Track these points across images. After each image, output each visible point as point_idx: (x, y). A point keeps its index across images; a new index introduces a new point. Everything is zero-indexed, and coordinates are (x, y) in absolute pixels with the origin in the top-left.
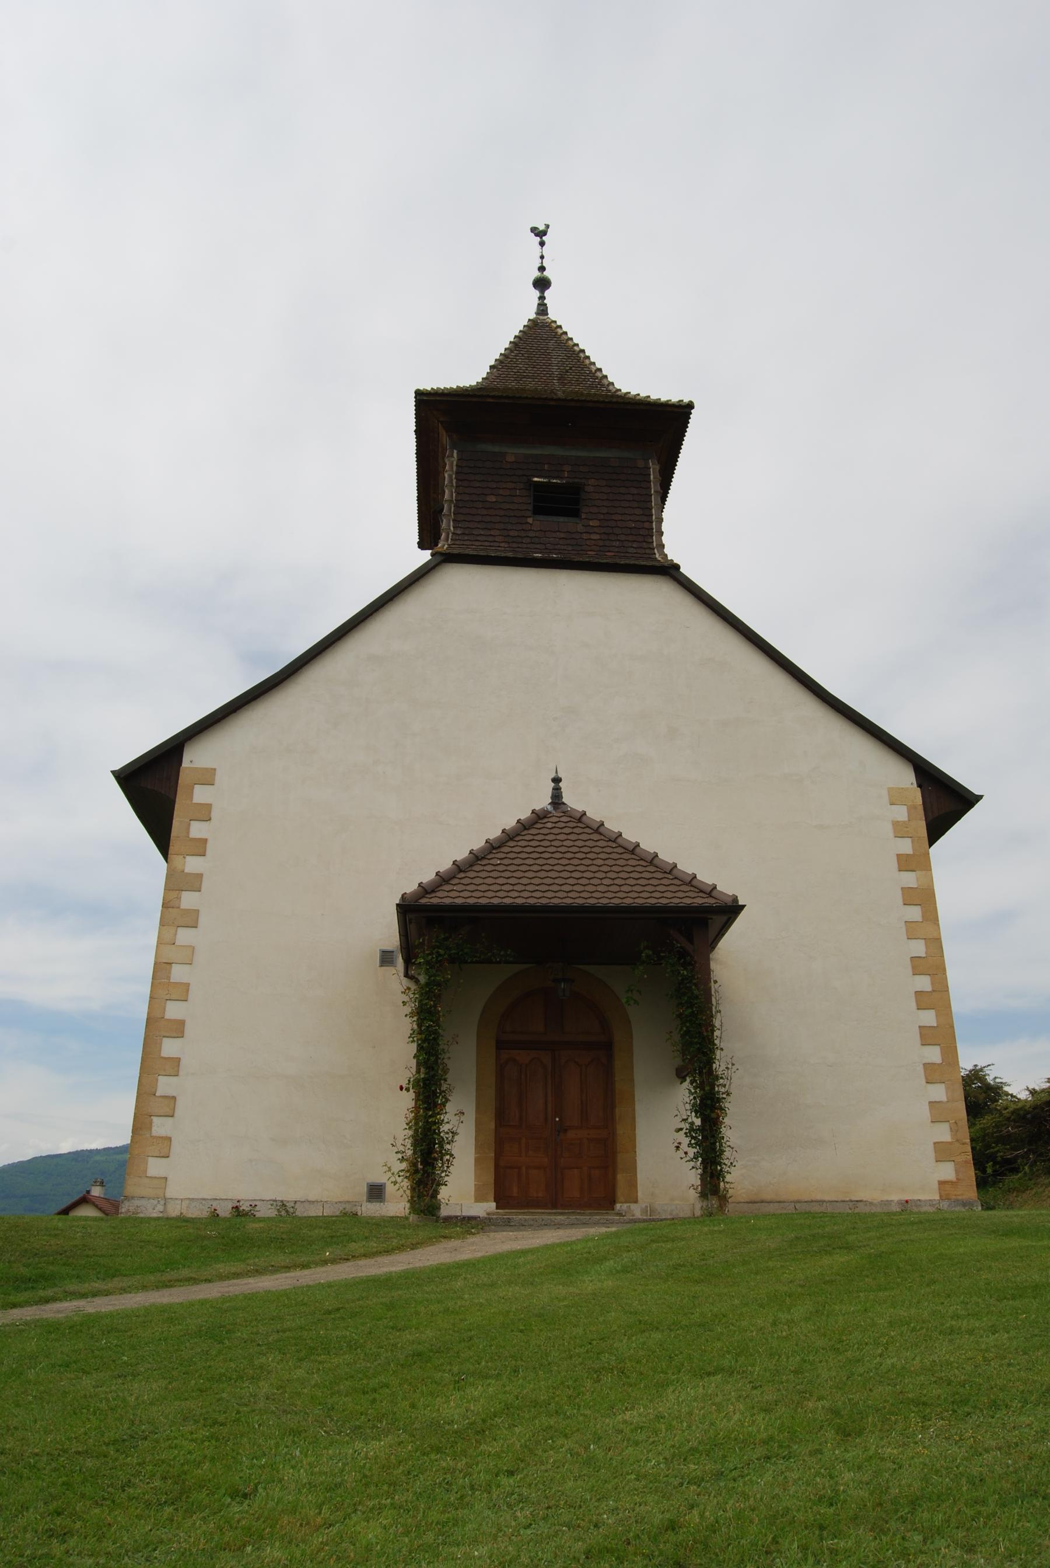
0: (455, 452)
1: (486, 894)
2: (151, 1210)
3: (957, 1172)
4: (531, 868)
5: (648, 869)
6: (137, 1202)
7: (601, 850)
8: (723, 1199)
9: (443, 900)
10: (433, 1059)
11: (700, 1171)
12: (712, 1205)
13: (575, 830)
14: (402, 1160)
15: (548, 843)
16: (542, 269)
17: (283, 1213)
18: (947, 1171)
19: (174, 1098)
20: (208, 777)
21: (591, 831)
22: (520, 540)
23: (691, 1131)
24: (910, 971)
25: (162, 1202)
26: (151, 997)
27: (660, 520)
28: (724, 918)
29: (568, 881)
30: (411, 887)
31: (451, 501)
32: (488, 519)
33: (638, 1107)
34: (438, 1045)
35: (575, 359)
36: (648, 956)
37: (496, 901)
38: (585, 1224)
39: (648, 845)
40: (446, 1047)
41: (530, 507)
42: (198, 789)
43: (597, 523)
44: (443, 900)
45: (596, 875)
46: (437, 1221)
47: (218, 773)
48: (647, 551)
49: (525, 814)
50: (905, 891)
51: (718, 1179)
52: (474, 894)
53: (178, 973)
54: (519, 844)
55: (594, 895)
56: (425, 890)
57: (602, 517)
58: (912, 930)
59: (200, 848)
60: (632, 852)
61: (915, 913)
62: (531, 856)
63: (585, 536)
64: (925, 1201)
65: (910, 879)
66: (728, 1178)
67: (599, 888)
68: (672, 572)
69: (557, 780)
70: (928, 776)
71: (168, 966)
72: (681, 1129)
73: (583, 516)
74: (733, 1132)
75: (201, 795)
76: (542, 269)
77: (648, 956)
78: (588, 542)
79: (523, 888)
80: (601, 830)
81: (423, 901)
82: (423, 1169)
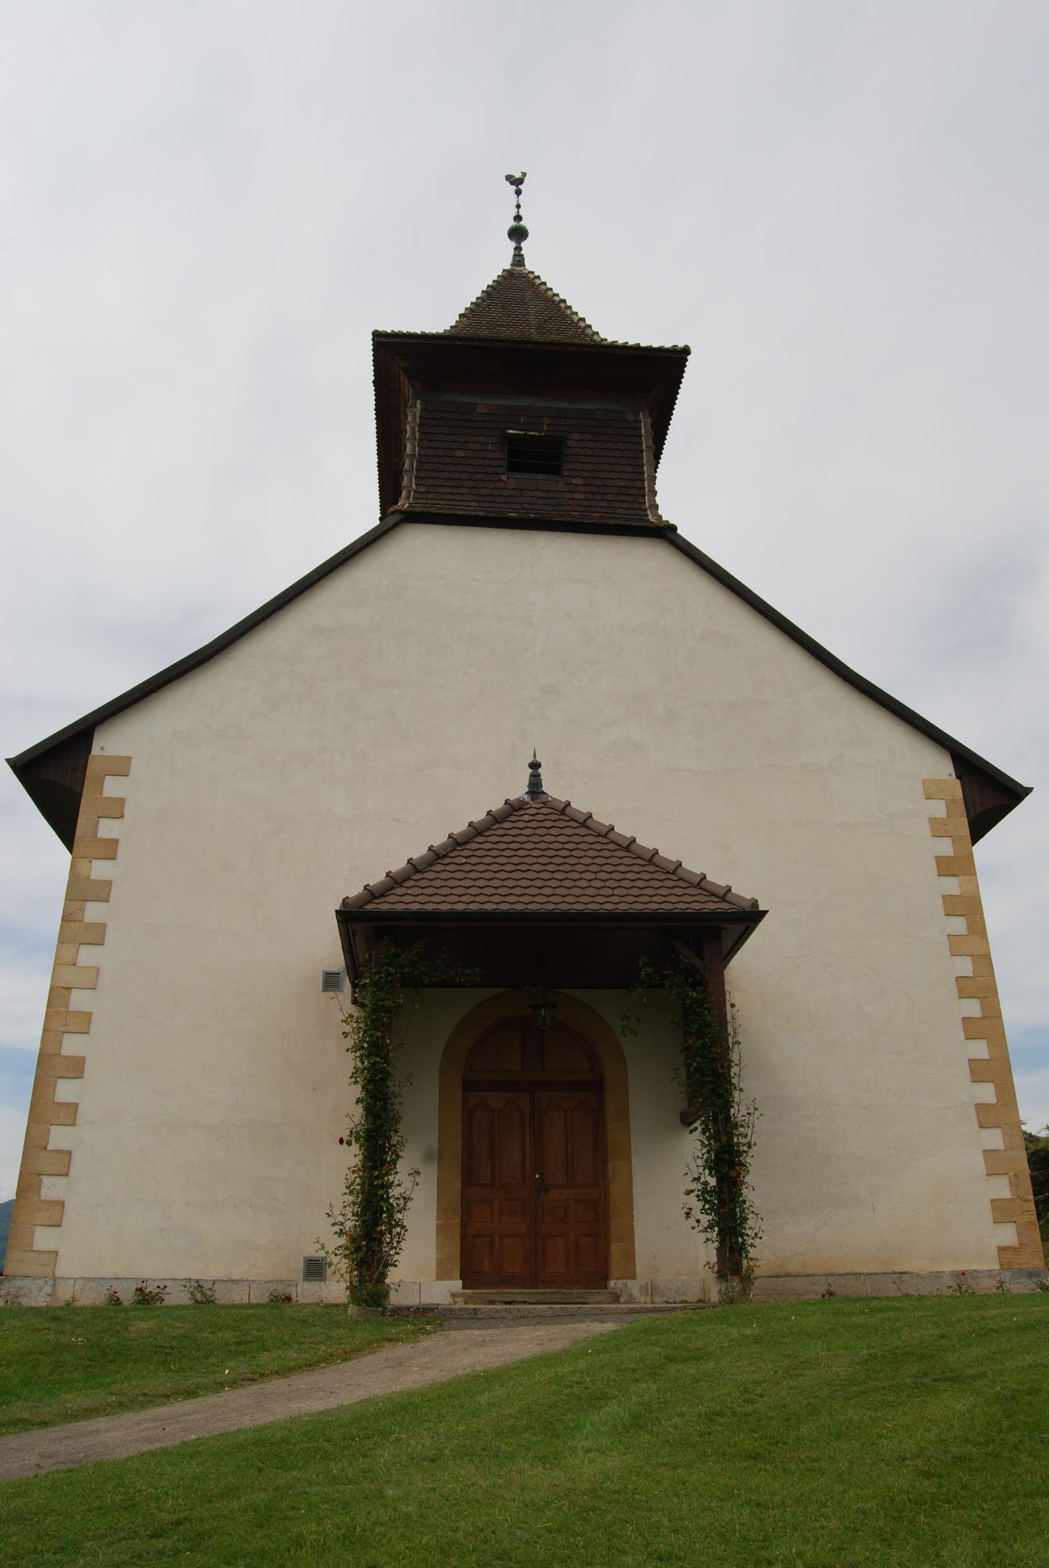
0: (419, 402)
1: (447, 899)
2: (37, 1297)
3: (1019, 1235)
4: (504, 868)
5: (646, 868)
6: (19, 1283)
7: (589, 846)
8: (747, 1280)
9: (394, 906)
10: (379, 1104)
11: (716, 1244)
12: (733, 1288)
13: (557, 824)
14: (341, 1233)
15: (525, 839)
16: (518, 218)
17: (199, 1296)
18: (1007, 1235)
19: (69, 1153)
20: (121, 767)
21: (576, 825)
22: (491, 499)
23: (704, 1194)
24: (955, 993)
25: (51, 1283)
26: (44, 1030)
27: (653, 480)
28: (741, 927)
29: (549, 883)
30: (355, 890)
31: (413, 456)
32: (457, 476)
33: (635, 1160)
34: (387, 1087)
35: (555, 309)
36: (648, 975)
37: (460, 907)
38: (573, 1316)
39: (646, 841)
40: (397, 1089)
41: (505, 463)
42: (109, 781)
43: (580, 481)
44: (394, 906)
45: (584, 876)
46: (383, 1315)
47: (133, 761)
48: (638, 512)
49: (497, 805)
50: (947, 899)
51: (740, 1255)
52: (433, 899)
53: (79, 1000)
54: (489, 839)
55: (581, 899)
56: (372, 894)
57: (587, 474)
58: (956, 946)
59: (109, 850)
60: (627, 848)
61: (959, 925)
62: (503, 853)
63: (567, 495)
64: (983, 1272)
65: (952, 885)
66: (752, 1253)
67: (588, 891)
68: (669, 534)
69: (535, 766)
70: (969, 766)
71: (66, 992)
72: (692, 1191)
73: (565, 473)
74: (757, 1191)
75: (112, 788)
76: (518, 218)
77: (648, 975)
78: (570, 502)
79: (494, 891)
80: (589, 823)
81: (369, 907)
82: (367, 1246)
